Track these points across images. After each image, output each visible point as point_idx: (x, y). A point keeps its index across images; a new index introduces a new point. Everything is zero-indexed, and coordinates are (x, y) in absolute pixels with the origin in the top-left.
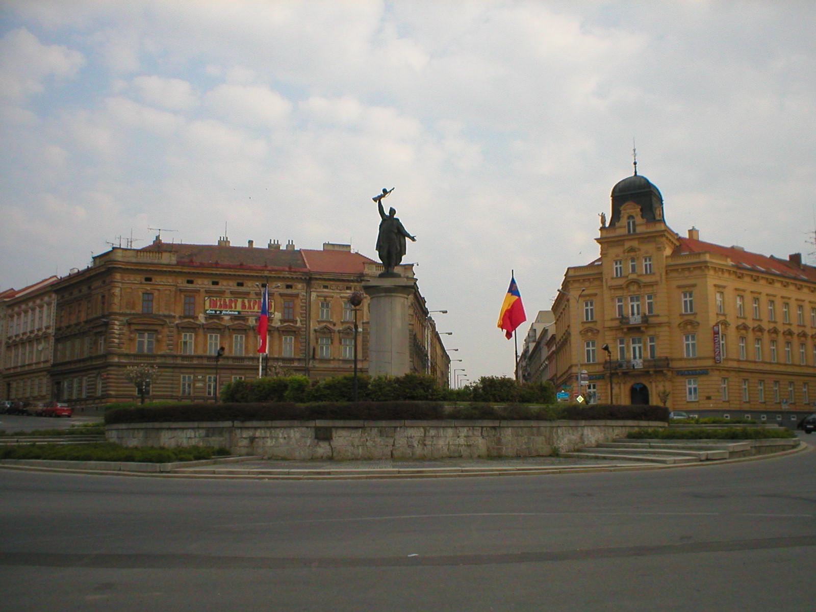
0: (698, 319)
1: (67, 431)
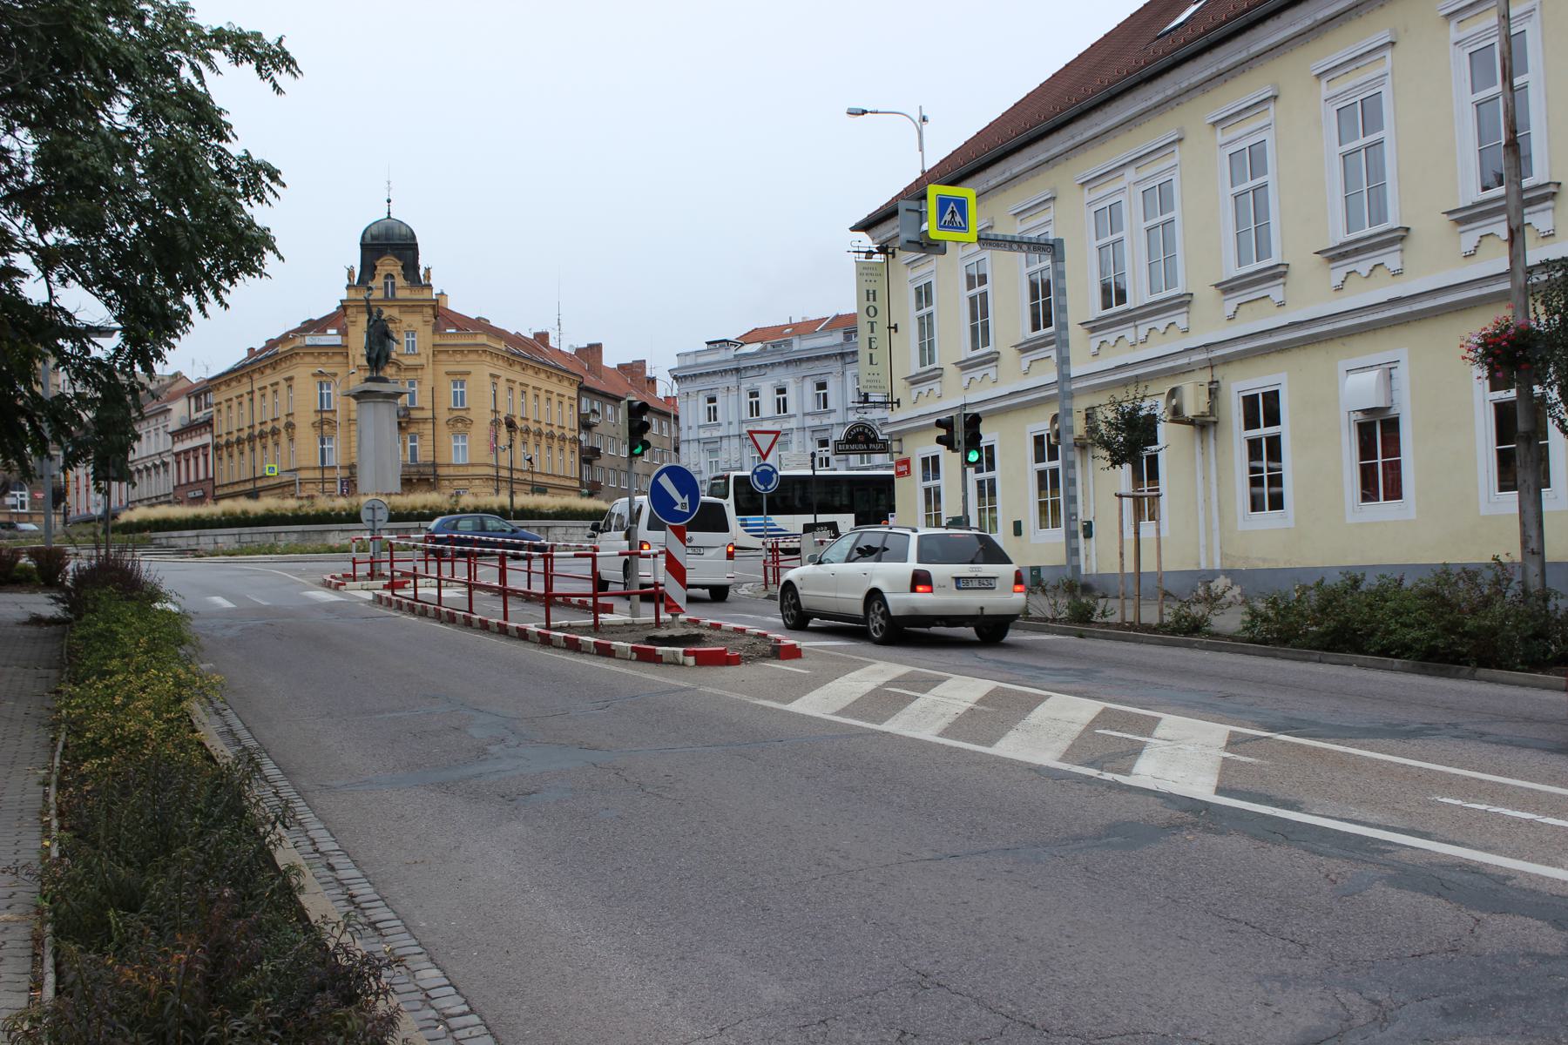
0: (472, 415)
1: (221, 602)
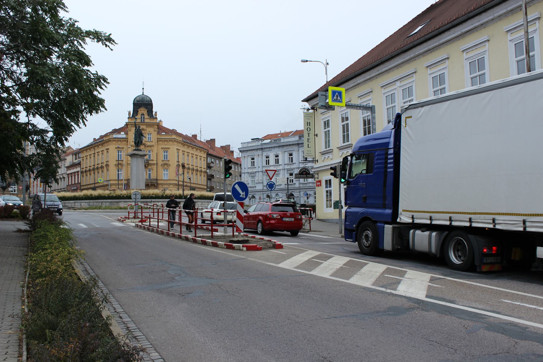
0: (170, 163)
